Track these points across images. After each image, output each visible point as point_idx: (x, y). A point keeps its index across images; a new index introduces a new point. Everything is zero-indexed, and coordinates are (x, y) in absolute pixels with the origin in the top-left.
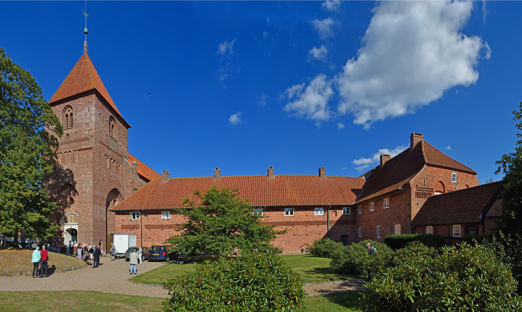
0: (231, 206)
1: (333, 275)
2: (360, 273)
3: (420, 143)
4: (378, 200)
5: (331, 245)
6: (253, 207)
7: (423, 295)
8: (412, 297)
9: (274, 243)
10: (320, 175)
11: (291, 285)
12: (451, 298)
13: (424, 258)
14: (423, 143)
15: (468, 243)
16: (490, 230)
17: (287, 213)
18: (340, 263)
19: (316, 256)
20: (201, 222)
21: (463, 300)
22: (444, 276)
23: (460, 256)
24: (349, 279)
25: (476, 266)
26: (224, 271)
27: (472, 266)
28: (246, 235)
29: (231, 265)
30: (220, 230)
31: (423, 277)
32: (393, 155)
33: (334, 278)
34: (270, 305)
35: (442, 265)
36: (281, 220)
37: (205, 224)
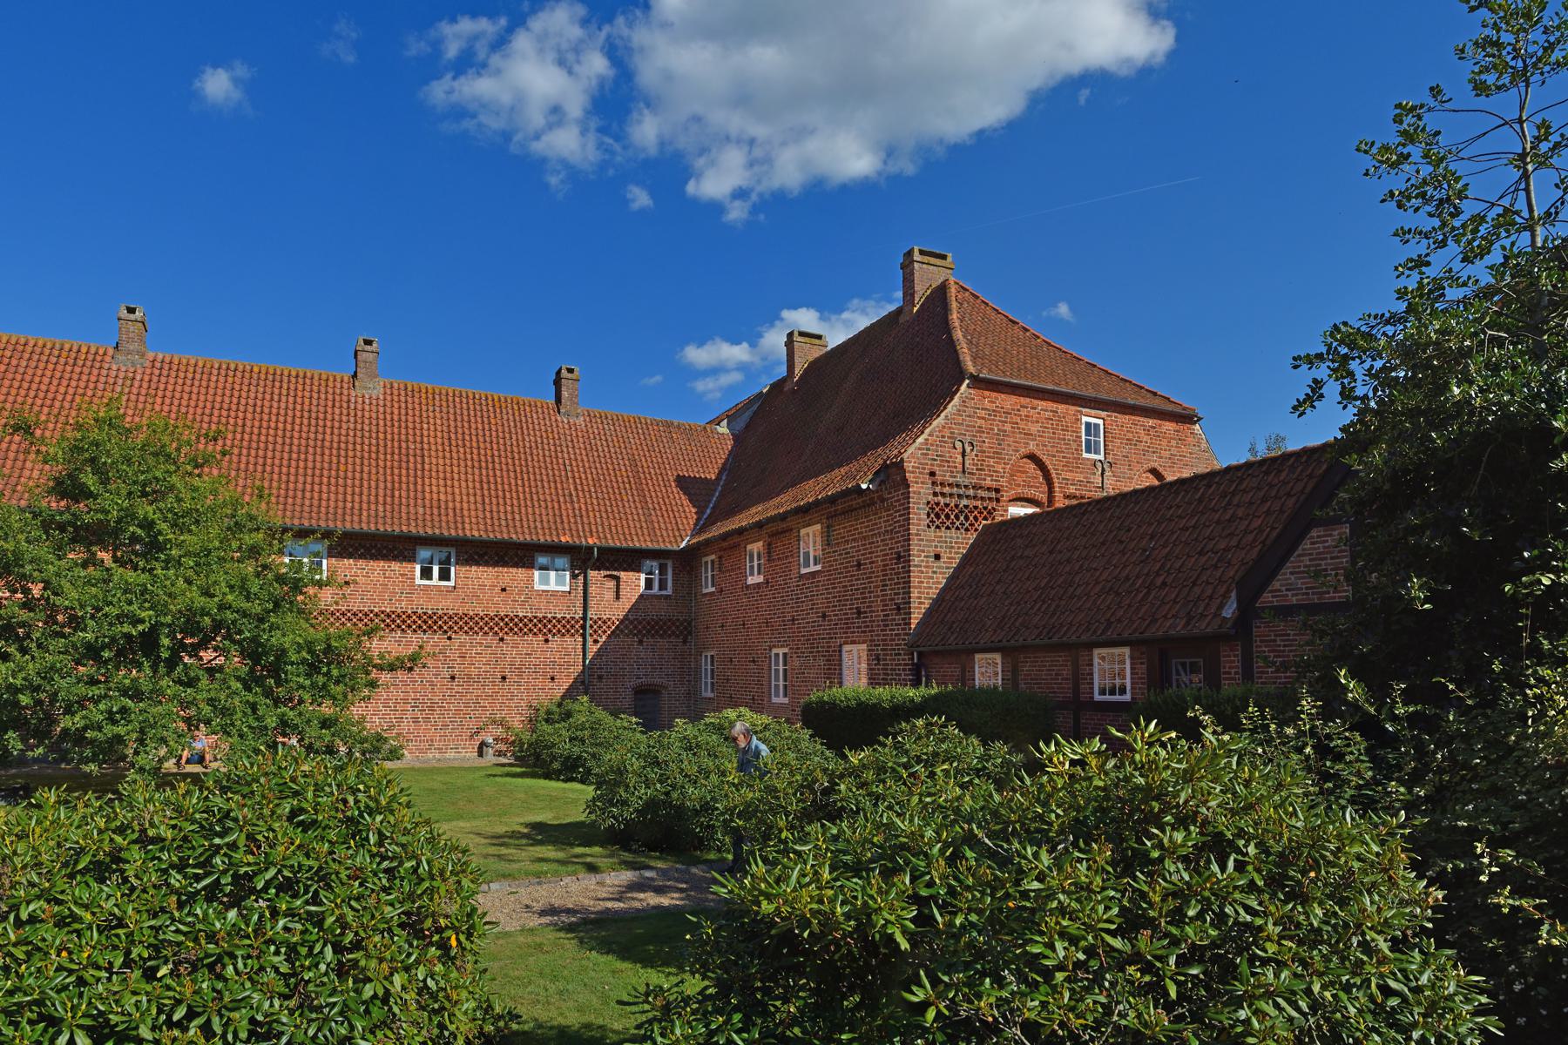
0: (188, 513)
1: (597, 849)
2: (700, 844)
3: (941, 291)
4: (779, 531)
5: (595, 727)
6: (285, 530)
7: (951, 924)
8: (904, 932)
9: (371, 713)
10: (558, 400)
11: (431, 891)
12: (1074, 941)
13: (962, 786)
14: (953, 290)
15: (1164, 727)
16: (1285, 666)
17: (426, 573)
18: (625, 803)
19: (534, 775)
20: (36, 590)
21: (1128, 948)
22: (1046, 859)
23: (1127, 779)
24: (660, 865)
25: (1205, 822)
26: (143, 840)
27: (1183, 822)
28: (252, 671)
29: (179, 810)
30: (128, 636)
31: (952, 861)
32: (836, 337)
33: (602, 862)
34: (341, 971)
35: (1041, 817)
36: (403, 606)
37: (58, 601)
